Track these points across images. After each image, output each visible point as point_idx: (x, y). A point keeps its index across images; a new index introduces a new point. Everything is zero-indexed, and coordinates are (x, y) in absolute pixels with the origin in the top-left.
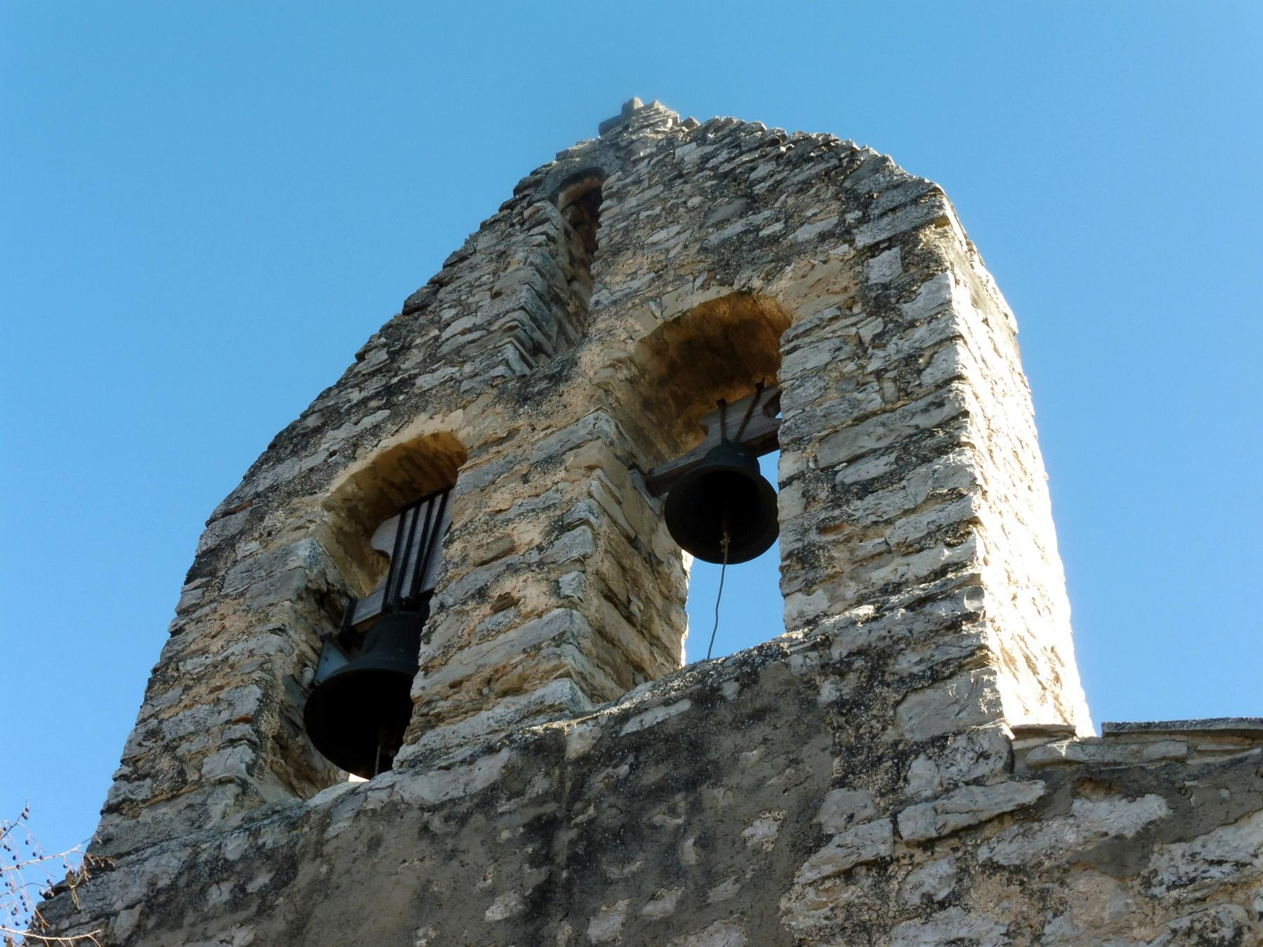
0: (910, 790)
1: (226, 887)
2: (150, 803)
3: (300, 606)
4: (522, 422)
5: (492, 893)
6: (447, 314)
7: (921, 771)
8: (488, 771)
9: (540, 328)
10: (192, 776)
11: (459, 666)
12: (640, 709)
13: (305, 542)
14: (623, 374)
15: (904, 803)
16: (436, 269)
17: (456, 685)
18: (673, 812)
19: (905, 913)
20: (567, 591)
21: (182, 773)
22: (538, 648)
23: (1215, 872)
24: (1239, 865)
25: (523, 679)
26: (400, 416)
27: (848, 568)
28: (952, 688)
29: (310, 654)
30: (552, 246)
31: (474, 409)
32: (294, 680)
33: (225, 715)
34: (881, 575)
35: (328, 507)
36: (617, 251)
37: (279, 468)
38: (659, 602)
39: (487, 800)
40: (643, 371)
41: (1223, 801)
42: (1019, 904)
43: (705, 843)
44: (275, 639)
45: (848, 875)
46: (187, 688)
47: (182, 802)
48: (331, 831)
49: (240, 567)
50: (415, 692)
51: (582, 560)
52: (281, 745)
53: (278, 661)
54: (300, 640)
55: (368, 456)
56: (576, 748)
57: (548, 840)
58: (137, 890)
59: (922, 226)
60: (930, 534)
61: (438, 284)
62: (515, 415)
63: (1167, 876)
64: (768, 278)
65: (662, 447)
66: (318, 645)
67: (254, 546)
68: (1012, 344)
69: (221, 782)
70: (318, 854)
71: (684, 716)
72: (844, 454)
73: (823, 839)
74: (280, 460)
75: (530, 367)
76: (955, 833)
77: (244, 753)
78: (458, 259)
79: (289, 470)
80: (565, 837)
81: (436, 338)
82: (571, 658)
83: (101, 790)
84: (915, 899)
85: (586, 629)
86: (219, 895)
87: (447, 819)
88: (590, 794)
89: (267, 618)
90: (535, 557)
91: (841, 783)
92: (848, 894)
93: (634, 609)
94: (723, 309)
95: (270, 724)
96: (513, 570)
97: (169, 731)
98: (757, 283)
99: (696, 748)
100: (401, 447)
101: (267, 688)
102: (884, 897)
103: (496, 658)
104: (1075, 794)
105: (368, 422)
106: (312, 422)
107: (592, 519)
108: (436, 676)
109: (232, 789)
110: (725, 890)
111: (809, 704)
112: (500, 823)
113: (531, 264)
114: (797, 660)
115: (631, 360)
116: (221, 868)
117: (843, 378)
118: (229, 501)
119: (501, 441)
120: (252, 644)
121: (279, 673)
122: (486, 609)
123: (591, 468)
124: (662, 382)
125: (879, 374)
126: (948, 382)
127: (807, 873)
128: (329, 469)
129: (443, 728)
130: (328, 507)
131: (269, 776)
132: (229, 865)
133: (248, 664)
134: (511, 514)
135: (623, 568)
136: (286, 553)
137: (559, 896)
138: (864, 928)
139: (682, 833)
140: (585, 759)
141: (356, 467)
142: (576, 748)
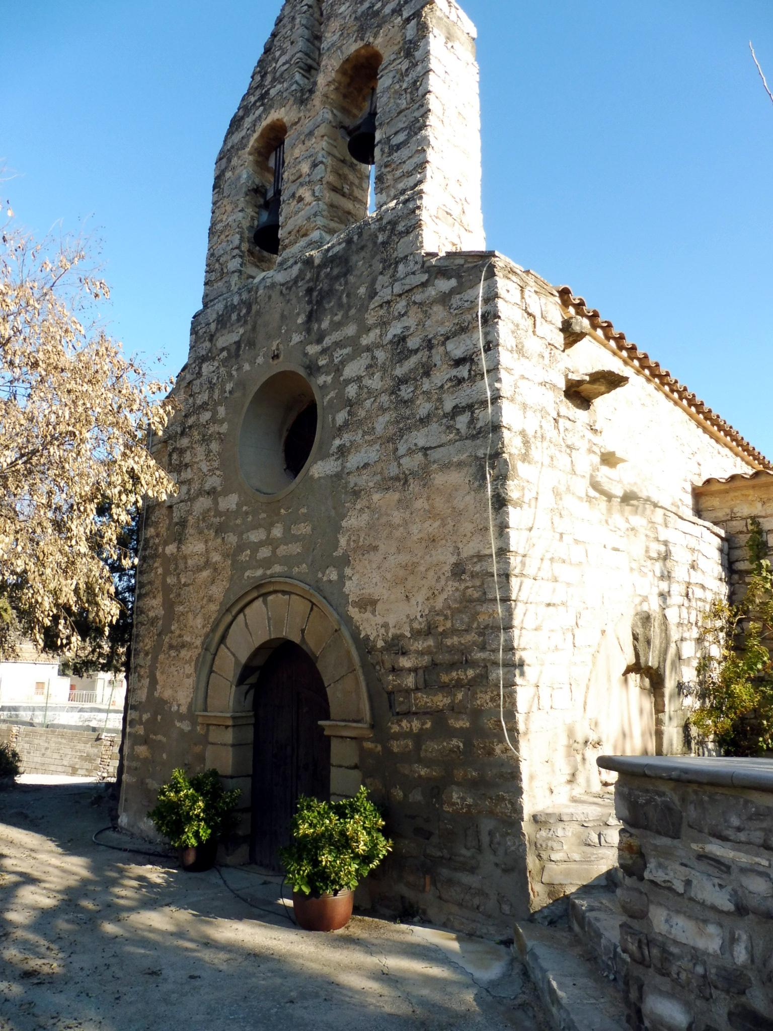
0: (398, 275)
1: (236, 314)
2: (216, 281)
3: (247, 198)
4: (302, 114)
5: (298, 314)
6: (278, 54)
7: (401, 267)
8: (295, 271)
9: (309, 57)
10: (225, 271)
11: (291, 225)
12: (333, 246)
13: (245, 171)
14: (332, 87)
15: (396, 281)
16: (271, 28)
17: (290, 233)
18: (341, 285)
19: (395, 318)
20: (317, 194)
21: (222, 269)
22: (309, 218)
23: (466, 304)
24: (472, 302)
25: (307, 230)
26: (266, 111)
27: (392, 182)
28: (411, 237)
29: (255, 215)
30: (311, 10)
31: (288, 107)
32: (251, 227)
33: (231, 246)
34: (401, 186)
35: (250, 154)
36: (329, 19)
37: (233, 137)
38: (356, 181)
39: (296, 281)
40: (340, 83)
41: (470, 280)
42: (421, 315)
43: (348, 296)
44: (241, 214)
45: (381, 306)
46: (219, 236)
47: (224, 280)
48: (259, 293)
49: (227, 184)
50: (279, 236)
51: (321, 180)
52: (251, 252)
53: (243, 222)
54: (250, 211)
55: (259, 130)
56: (317, 262)
57: (311, 295)
58: (214, 316)
59: (423, 7)
60: (414, 168)
61: (274, 35)
62: (300, 111)
63: (455, 306)
64: (376, 36)
65: (355, 111)
66: (257, 210)
67: (230, 173)
68: (470, 48)
69: (233, 272)
70: (256, 302)
71: (344, 249)
72: (393, 130)
73: (376, 293)
74: (233, 133)
75: (308, 79)
76: (407, 292)
77: (238, 260)
78: (279, 20)
79: (236, 138)
80: (315, 294)
81: (275, 68)
82: (320, 221)
83: (201, 277)
84: (397, 314)
85: (325, 207)
86: (234, 317)
87: (287, 289)
88: (321, 279)
89: (237, 206)
90: (307, 179)
91: (381, 273)
92: (381, 312)
93: (346, 190)
94: (363, 51)
95: (245, 246)
96: (302, 185)
97: (217, 253)
98: (371, 40)
99: (347, 261)
100: (268, 125)
101: (241, 234)
102: (389, 313)
103: (299, 222)
104: (436, 278)
105: (258, 113)
106: (241, 113)
107: (324, 160)
108: (284, 230)
109: (236, 274)
110: (353, 312)
111: (375, 243)
112: (299, 289)
113: (303, 25)
114: (373, 226)
115: (334, 80)
116: (234, 308)
117: (396, 92)
118: (220, 153)
119: (296, 123)
120: (234, 217)
121: (245, 227)
122: (295, 202)
123: (323, 136)
124: (349, 85)
125: (405, 90)
126: (425, 94)
127: (372, 306)
128: (247, 137)
129: (288, 250)
130: (250, 154)
131: (248, 265)
132: (235, 306)
133: (235, 225)
134: (300, 159)
135: (339, 175)
136: (239, 177)
137: (314, 314)
138: (384, 323)
139: (342, 293)
140: (319, 266)
141: (256, 135)
142: (317, 262)
